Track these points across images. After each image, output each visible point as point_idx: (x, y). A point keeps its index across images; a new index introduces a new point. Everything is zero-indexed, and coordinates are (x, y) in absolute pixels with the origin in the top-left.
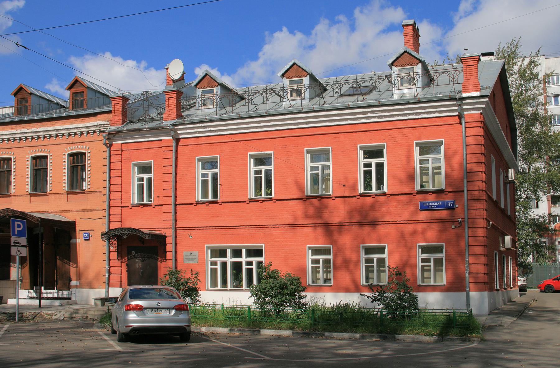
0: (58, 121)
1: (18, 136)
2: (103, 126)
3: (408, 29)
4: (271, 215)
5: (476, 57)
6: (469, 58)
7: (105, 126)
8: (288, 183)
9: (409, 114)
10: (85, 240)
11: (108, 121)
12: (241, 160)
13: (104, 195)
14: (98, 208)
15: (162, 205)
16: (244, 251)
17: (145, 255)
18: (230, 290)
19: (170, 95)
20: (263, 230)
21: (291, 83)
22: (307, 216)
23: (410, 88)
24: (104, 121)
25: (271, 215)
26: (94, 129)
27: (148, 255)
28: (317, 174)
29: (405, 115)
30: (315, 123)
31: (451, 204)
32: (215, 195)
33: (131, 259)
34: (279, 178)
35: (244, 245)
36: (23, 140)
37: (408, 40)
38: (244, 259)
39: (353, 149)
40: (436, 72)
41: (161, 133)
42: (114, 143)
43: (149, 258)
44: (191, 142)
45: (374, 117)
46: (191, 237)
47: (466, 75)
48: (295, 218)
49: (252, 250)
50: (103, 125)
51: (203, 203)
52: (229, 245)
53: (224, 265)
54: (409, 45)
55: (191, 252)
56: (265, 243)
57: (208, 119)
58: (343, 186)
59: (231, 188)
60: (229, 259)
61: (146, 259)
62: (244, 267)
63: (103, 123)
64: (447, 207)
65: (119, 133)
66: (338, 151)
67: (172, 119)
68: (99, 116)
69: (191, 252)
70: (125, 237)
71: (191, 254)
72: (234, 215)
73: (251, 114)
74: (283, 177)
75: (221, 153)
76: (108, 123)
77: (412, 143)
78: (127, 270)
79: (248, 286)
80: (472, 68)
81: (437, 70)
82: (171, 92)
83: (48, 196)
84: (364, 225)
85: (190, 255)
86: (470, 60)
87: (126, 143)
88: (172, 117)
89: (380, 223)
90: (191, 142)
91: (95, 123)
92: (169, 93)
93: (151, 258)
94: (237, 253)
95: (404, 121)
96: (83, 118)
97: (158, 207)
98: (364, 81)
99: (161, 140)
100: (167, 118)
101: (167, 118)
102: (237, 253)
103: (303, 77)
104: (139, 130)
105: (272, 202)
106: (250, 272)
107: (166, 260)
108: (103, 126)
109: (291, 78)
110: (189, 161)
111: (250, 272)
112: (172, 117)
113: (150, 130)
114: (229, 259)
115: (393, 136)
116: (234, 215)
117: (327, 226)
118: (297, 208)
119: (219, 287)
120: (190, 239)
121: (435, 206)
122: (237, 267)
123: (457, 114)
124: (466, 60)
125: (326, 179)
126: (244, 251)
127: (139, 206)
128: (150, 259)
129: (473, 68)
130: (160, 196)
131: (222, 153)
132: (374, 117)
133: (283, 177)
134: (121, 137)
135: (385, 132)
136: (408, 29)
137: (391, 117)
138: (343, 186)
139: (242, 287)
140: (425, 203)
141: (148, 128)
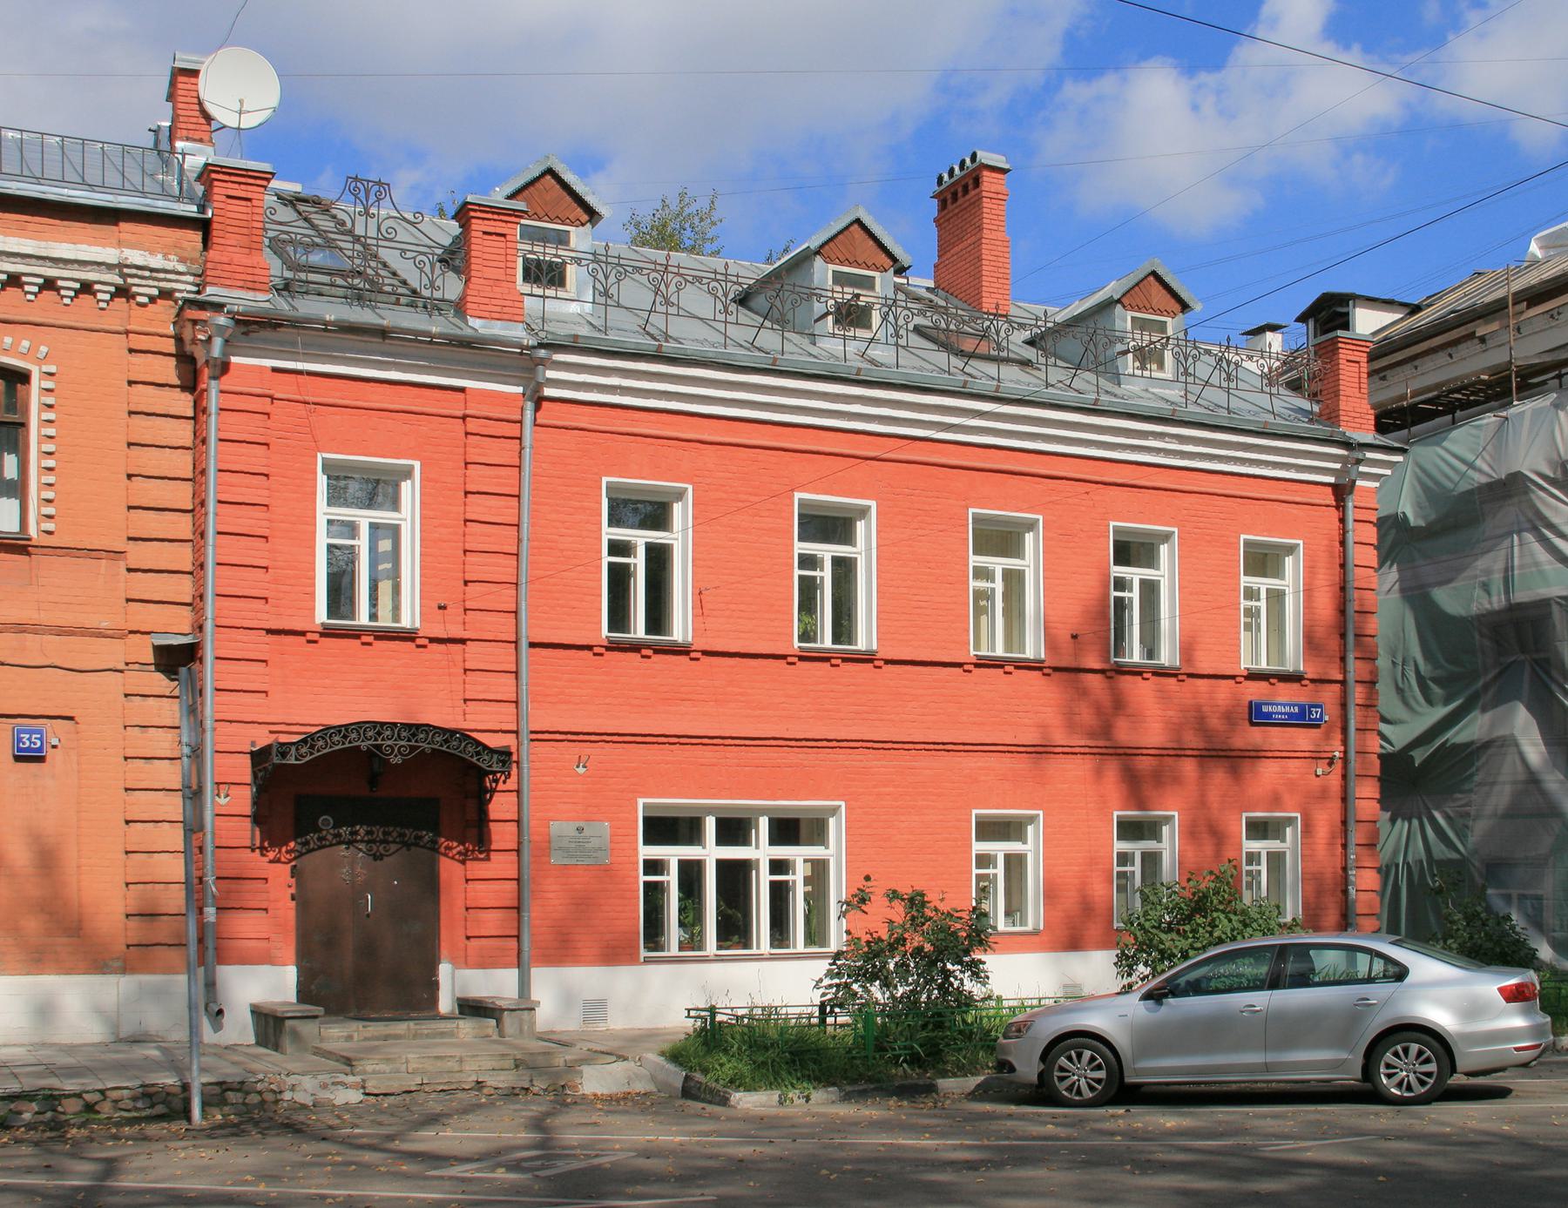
0: (57, 222)
1: (77, 275)
2: (147, 274)
3: (995, 181)
4: (865, 708)
5: (1368, 344)
6: (1354, 342)
7: (162, 275)
8: (919, 611)
9: (1243, 461)
10: (18, 759)
11: (182, 260)
12: (767, 514)
13: (129, 570)
14: (104, 625)
15: (463, 641)
16: (710, 825)
17: (389, 834)
18: (719, 959)
19: (492, 223)
20: (841, 757)
21: (839, 278)
22: (1071, 725)
23: (556, 298)
24: (160, 256)
25: (865, 708)
26: (90, 276)
27: (402, 835)
28: (352, 551)
29: (1243, 461)
30: (698, 403)
31: (1317, 712)
32: (658, 617)
33: (320, 848)
34: (892, 589)
35: (763, 805)
36: (100, 296)
37: (993, 212)
38: (760, 851)
39: (1098, 534)
40: (616, 261)
41: (472, 364)
42: (234, 359)
43: (407, 845)
44: (583, 418)
45: (1158, 451)
46: (581, 770)
47: (509, 271)
48: (1043, 727)
49: (684, 819)
50: (152, 270)
51: (614, 647)
52: (710, 803)
53: (691, 874)
54: (995, 228)
55: (582, 824)
56: (847, 797)
57: (664, 349)
58: (440, 608)
59: (733, 607)
60: (711, 852)
61: (393, 847)
62: (763, 880)
63: (156, 261)
64: (1310, 719)
65: (281, 325)
66: (1060, 531)
67: (505, 316)
68: (123, 225)
69: (582, 824)
70: (396, 760)
71: (581, 830)
72: (742, 699)
73: (1222, 417)
74: (905, 590)
75: (696, 479)
76: (181, 268)
77: (1232, 540)
78: (293, 890)
79: (811, 939)
80: (498, 243)
81: (679, 267)
82: (498, 214)
83: (29, 554)
84: (1183, 758)
85: (577, 834)
86: (1354, 348)
87: (310, 373)
88: (505, 310)
89: (1270, 754)
90: (583, 418)
91: (110, 255)
92: (490, 216)
93: (417, 845)
94: (733, 830)
95: (1220, 477)
96: (32, 215)
97: (442, 647)
98: (630, 269)
99: (462, 390)
100: (482, 307)
101: (482, 307)
102: (733, 830)
103: (572, 224)
104: (383, 333)
105: (302, 639)
106: (780, 894)
107: (488, 851)
108: (147, 274)
109: (842, 263)
110: (576, 489)
111: (780, 894)
112: (505, 310)
113: (431, 343)
114: (711, 852)
115: (1193, 513)
116: (742, 699)
117: (1124, 754)
118: (1043, 698)
119: (800, 946)
120: (578, 775)
121: (1285, 714)
122: (735, 877)
123: (1331, 480)
124: (1348, 347)
125: (387, 567)
126: (710, 825)
127: (358, 637)
128: (413, 848)
129: (249, 210)
130: (450, 604)
131: (700, 479)
132: (1158, 451)
133: (905, 590)
134: (294, 344)
135: (1174, 497)
136: (995, 181)
137: (1193, 459)
138: (440, 608)
139: (701, 947)
140: (1266, 704)
141: (440, 336)
